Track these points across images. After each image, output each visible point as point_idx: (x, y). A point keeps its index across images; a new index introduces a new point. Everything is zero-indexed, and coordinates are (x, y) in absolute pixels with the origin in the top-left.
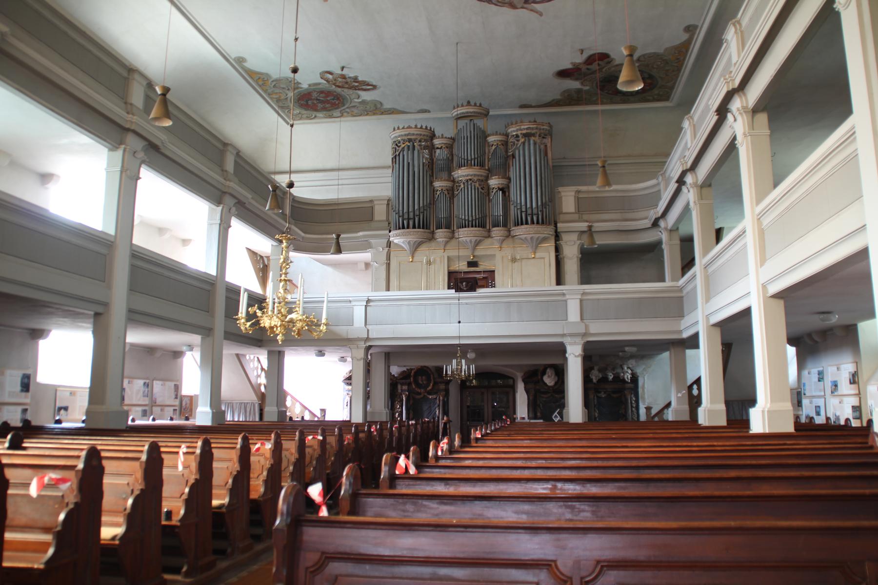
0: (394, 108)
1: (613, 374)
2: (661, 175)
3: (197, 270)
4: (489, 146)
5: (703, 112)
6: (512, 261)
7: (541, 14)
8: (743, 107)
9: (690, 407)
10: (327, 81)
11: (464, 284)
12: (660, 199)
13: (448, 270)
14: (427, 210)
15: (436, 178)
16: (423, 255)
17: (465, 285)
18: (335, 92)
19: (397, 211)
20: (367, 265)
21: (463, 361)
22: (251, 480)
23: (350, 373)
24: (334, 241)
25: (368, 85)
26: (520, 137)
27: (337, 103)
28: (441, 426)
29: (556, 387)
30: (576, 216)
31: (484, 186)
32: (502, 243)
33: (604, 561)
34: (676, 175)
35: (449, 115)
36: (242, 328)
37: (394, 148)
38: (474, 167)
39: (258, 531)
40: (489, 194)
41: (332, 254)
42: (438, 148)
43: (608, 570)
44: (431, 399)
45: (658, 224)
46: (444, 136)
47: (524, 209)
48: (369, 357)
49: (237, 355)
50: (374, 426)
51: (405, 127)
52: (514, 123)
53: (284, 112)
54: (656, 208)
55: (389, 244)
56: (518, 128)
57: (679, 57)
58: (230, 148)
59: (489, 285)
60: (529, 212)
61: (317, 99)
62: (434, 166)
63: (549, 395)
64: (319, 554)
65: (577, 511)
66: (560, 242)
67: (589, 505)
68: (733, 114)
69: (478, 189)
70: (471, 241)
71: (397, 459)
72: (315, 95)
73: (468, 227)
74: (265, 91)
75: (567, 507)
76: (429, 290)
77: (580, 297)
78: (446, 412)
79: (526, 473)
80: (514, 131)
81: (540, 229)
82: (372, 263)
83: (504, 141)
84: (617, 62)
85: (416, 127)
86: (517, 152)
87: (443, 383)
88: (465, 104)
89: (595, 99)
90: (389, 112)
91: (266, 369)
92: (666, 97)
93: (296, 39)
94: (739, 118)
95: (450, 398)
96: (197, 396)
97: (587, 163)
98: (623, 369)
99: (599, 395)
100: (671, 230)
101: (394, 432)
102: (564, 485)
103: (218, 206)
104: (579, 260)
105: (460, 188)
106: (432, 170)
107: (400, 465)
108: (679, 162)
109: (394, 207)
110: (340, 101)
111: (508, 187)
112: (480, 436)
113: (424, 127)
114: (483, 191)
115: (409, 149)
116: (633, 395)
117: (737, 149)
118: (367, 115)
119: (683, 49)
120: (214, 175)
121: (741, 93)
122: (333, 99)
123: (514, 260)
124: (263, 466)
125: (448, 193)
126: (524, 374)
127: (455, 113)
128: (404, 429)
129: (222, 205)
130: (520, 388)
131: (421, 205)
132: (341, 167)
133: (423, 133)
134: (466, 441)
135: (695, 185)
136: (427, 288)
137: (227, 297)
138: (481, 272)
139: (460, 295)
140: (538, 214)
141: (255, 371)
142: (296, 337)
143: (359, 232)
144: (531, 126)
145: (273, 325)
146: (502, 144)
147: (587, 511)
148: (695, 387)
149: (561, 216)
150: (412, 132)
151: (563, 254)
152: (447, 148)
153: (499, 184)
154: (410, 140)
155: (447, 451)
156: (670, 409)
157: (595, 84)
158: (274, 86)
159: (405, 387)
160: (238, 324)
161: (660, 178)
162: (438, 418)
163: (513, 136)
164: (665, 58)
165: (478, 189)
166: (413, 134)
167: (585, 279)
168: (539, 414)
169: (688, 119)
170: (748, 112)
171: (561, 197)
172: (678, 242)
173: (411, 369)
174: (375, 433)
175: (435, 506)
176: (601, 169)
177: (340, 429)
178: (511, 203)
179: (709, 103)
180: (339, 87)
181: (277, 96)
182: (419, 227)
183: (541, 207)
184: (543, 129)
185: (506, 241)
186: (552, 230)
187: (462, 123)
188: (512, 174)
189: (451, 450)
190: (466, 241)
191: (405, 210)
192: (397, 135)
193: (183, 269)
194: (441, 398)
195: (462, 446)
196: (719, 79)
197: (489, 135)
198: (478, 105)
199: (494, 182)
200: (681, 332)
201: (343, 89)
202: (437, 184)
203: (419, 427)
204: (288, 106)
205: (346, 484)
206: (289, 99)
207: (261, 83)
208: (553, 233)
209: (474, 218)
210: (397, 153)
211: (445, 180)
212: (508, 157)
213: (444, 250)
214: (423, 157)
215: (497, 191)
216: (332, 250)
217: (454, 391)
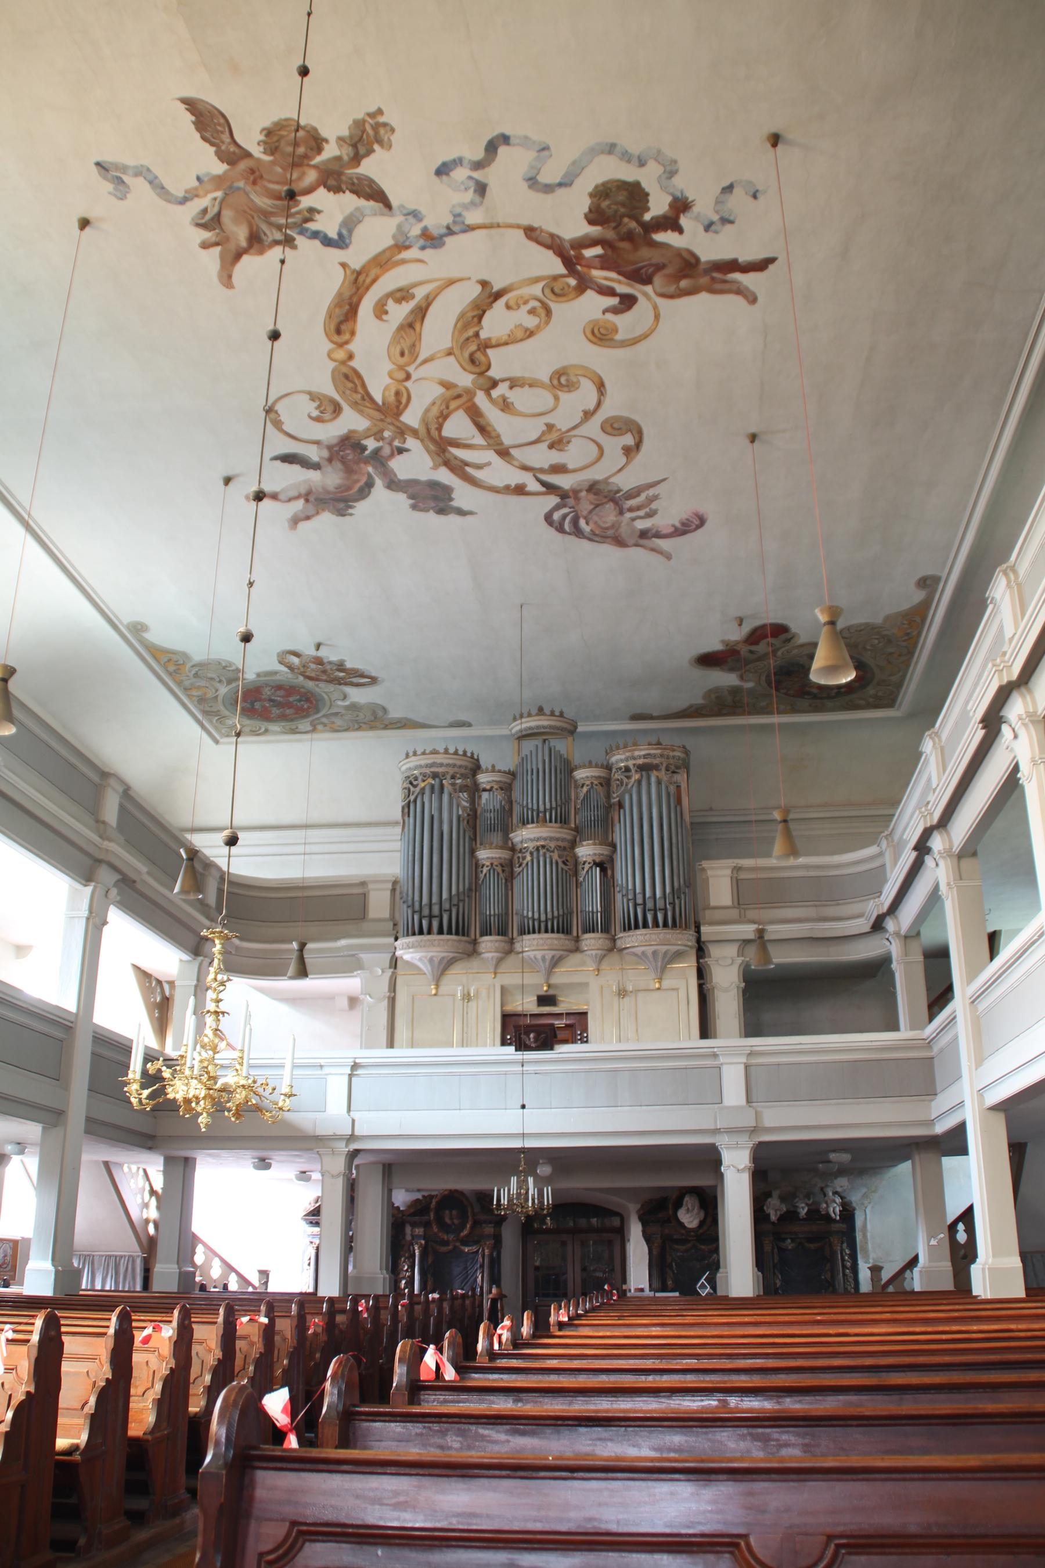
0: (406, 718)
1: (807, 1204)
2: (886, 837)
3: (40, 1000)
4: (576, 787)
5: (956, 723)
6: (619, 994)
7: (668, 557)
8: (1029, 715)
9: (953, 1265)
10: (291, 668)
11: (532, 1036)
12: (885, 881)
13: (502, 1011)
14: (464, 901)
15: (481, 844)
16: (456, 982)
17: (534, 1038)
18: (303, 687)
19: (410, 903)
20: (353, 1001)
21: (531, 1180)
22: (132, 1399)
23: (317, 1202)
24: (294, 956)
25: (363, 676)
26: (633, 771)
27: (305, 706)
28: (487, 1305)
29: (701, 1231)
30: (734, 913)
31: (568, 858)
32: (600, 961)
33: (841, 1536)
34: (913, 836)
35: (506, 732)
36: (133, 1100)
37: (405, 788)
38: (550, 824)
39: (139, 1504)
40: (576, 874)
41: (291, 978)
42: (485, 790)
43: (850, 1554)
44: (468, 1253)
45: (884, 925)
46: (497, 768)
47: (639, 901)
48: (354, 1171)
49: (106, 1164)
50: (363, 1301)
51: (427, 752)
52: (621, 746)
53: (211, 722)
54: (879, 897)
55: (394, 962)
56: (628, 754)
57: (909, 631)
58: (112, 781)
59: (576, 1037)
60: (650, 905)
61: (271, 700)
62: (478, 821)
63: (690, 1245)
64: (288, 1524)
65: (774, 1445)
66: (706, 960)
67: (798, 1435)
68: (1010, 726)
69: (557, 863)
70: (544, 958)
71: (424, 1351)
72: (267, 692)
73: (539, 932)
74: (179, 684)
75: (755, 1438)
76: (467, 1046)
77: (744, 1060)
78: (495, 1279)
79: (666, 1380)
80: (622, 761)
81: (669, 936)
82: (362, 997)
83: (604, 778)
84: (803, 639)
85: (446, 752)
86: (627, 797)
87: (490, 1222)
88: (534, 711)
89: (763, 704)
90: (399, 725)
91: (160, 1191)
92: (889, 701)
93: (251, 584)
94: (1022, 733)
95: (503, 1251)
96: (27, 1241)
97: (753, 818)
98: (825, 1195)
99: (783, 1245)
100: (906, 937)
101: (400, 1314)
102: (742, 1401)
103: (85, 886)
104: (741, 994)
105: (525, 862)
106: (474, 828)
107: (425, 1363)
108: (917, 812)
109: (404, 895)
110: (311, 703)
111: (611, 860)
112: (566, 1319)
113: (461, 752)
114: (565, 868)
115: (432, 791)
116: (845, 1245)
117: (1022, 787)
118: (359, 729)
119: (917, 616)
120: (80, 829)
121: (1023, 689)
122: (300, 701)
123: (622, 993)
124: (154, 1372)
125: (503, 871)
126: (642, 1206)
127: (517, 727)
128: (418, 1308)
129: (93, 884)
130: (635, 1232)
131: (454, 892)
132: (310, 821)
133: (459, 763)
134: (541, 1327)
135: (948, 853)
136: (463, 1044)
137: (93, 1054)
138: (562, 1014)
139: (525, 1057)
140: (665, 910)
141: (139, 1196)
142: (233, 1119)
143: (339, 939)
144: (652, 752)
145: (190, 1096)
146: (601, 784)
147: (794, 1445)
148: (961, 1227)
149: (707, 912)
150: (439, 761)
151: (711, 981)
152: (502, 789)
153: (595, 854)
154: (435, 776)
155: (509, 1342)
156: (916, 1270)
157: (763, 678)
158: (196, 675)
159: (419, 1231)
160: (126, 1092)
161: (884, 844)
162: (482, 1288)
163: (620, 769)
164: (886, 633)
165: (557, 863)
166: (441, 765)
167: (752, 1028)
168: (670, 1283)
169: (931, 738)
170: (1038, 722)
171: (707, 879)
172: (921, 958)
173: (431, 1197)
174: (366, 1315)
175: (503, 1437)
176: (780, 826)
177: (301, 1305)
178: (618, 889)
179: (969, 708)
180: (310, 678)
181: (199, 693)
182: (450, 932)
183: (671, 896)
184: (674, 757)
185: (606, 959)
186: (691, 937)
187: (529, 746)
188: (618, 837)
189: (517, 1341)
190: (535, 958)
191: (425, 900)
192: (411, 765)
193: (17, 999)
194: (487, 1252)
195: (534, 1336)
196: (984, 667)
197: (576, 768)
198: (557, 713)
199: (586, 851)
200: (931, 1123)
201: (317, 683)
202: (484, 855)
203: (446, 1306)
204: (219, 711)
205: (332, 1394)
206: (220, 699)
207: (171, 668)
208: (692, 942)
209: (550, 916)
210: (412, 798)
211: (497, 847)
212: (610, 806)
213: (495, 973)
214: (458, 806)
215: (591, 867)
216: (292, 970)
217: (510, 1237)
